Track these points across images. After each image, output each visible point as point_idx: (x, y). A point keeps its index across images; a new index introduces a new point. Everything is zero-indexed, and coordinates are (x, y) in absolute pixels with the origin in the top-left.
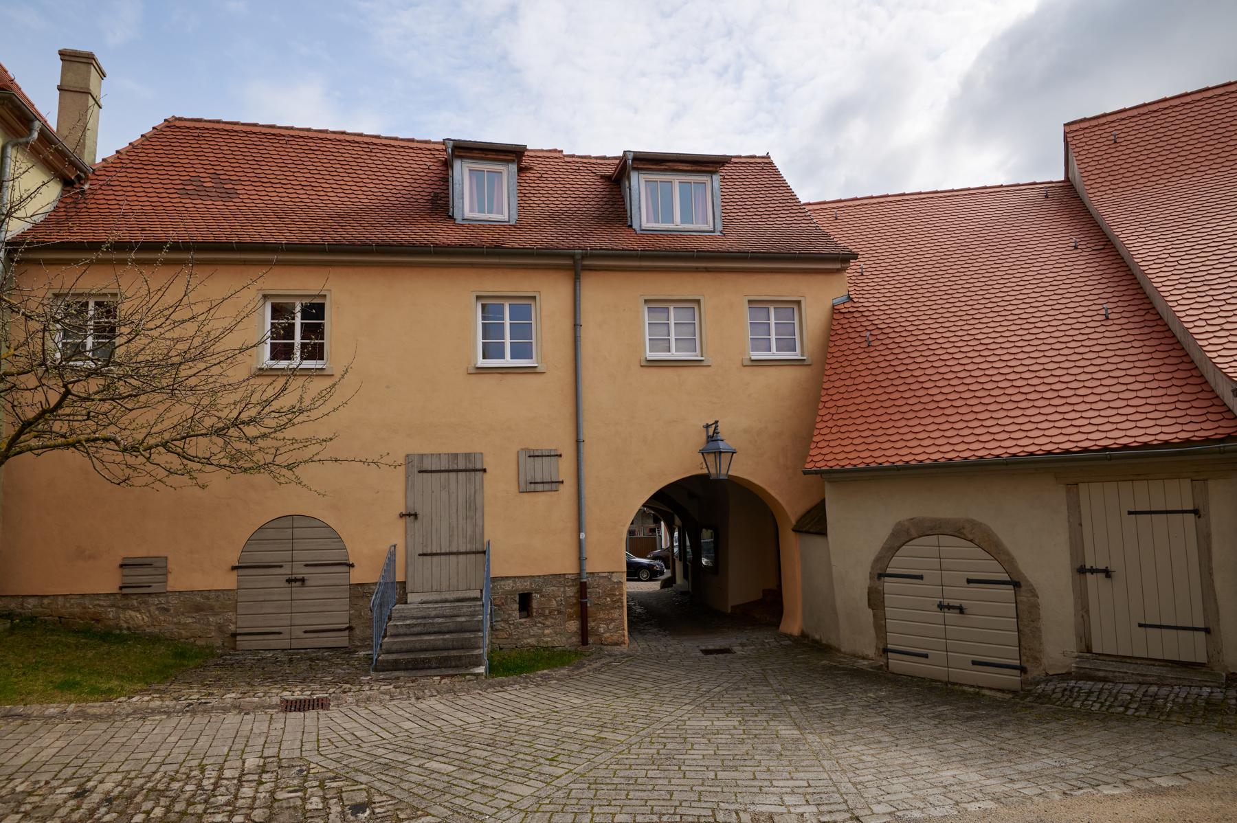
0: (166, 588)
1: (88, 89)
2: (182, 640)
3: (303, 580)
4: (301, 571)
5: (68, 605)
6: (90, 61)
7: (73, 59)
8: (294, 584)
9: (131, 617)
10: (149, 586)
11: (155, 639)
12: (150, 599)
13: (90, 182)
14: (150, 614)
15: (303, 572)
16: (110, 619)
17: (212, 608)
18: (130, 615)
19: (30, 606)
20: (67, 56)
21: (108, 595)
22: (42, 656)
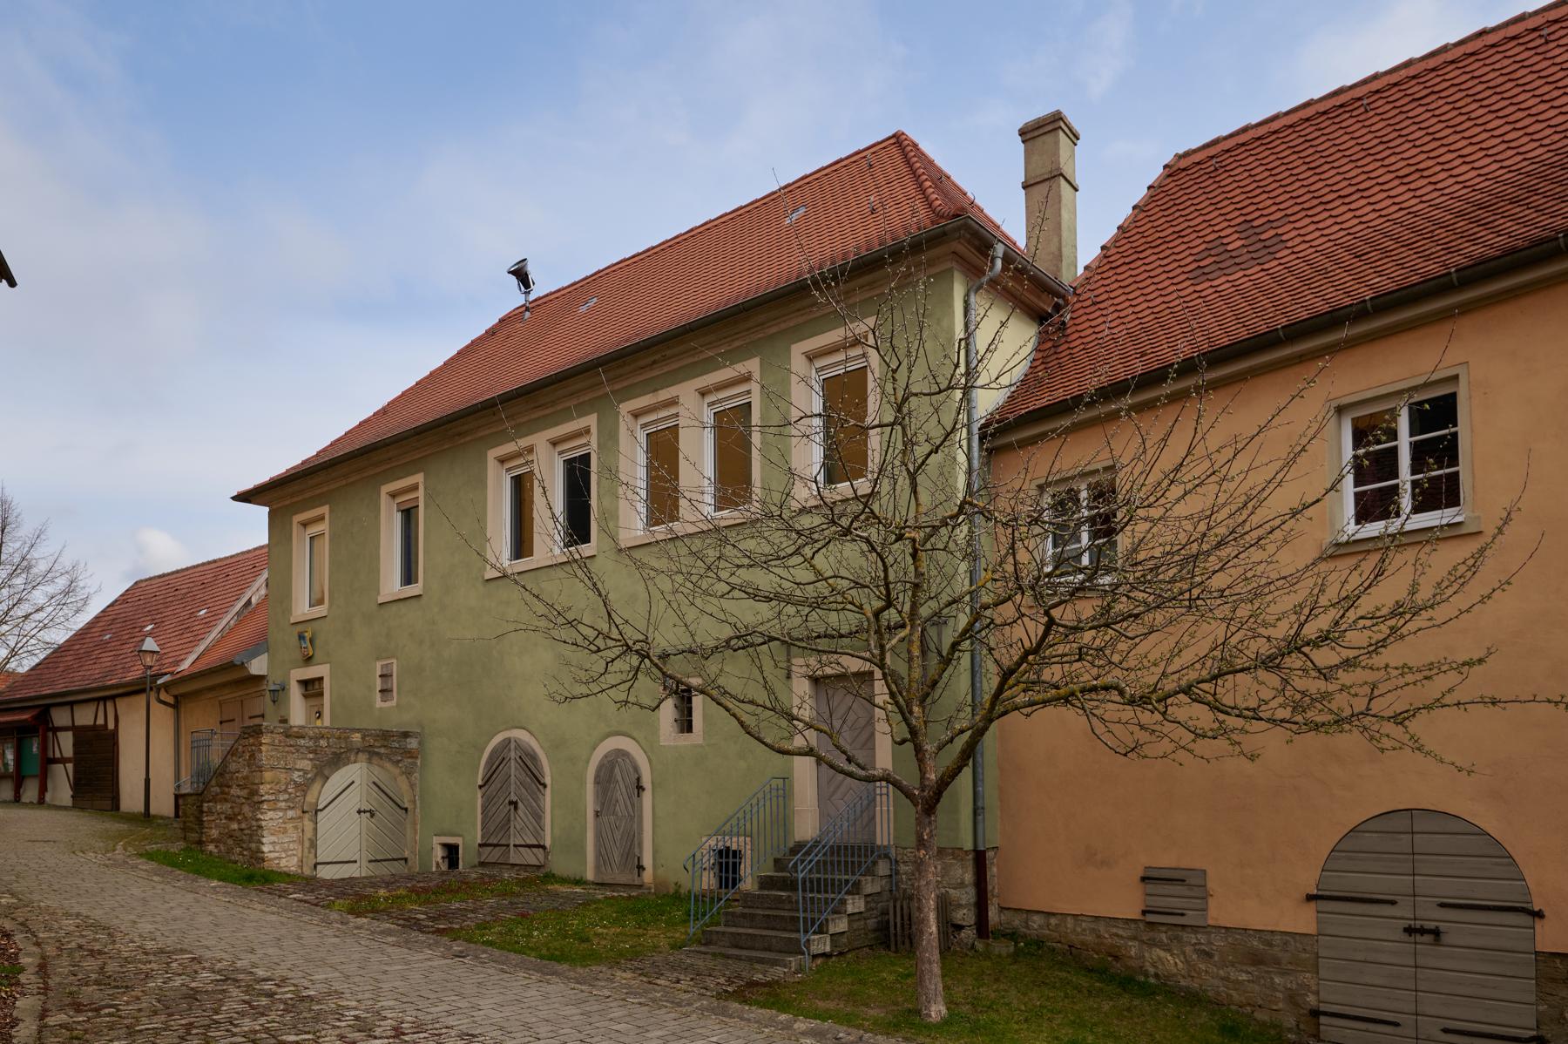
0: (1206, 919)
1: (1059, 168)
3: (1436, 933)
4: (1431, 916)
5: (1079, 930)
7: (1036, 133)
8: (1419, 938)
9: (1160, 959)
10: (1182, 915)
11: (1193, 999)
12: (1185, 935)
14: (1185, 957)
16: (1131, 957)
17: (1277, 962)
19: (1035, 926)
21: (1127, 921)
22: (1048, 999)
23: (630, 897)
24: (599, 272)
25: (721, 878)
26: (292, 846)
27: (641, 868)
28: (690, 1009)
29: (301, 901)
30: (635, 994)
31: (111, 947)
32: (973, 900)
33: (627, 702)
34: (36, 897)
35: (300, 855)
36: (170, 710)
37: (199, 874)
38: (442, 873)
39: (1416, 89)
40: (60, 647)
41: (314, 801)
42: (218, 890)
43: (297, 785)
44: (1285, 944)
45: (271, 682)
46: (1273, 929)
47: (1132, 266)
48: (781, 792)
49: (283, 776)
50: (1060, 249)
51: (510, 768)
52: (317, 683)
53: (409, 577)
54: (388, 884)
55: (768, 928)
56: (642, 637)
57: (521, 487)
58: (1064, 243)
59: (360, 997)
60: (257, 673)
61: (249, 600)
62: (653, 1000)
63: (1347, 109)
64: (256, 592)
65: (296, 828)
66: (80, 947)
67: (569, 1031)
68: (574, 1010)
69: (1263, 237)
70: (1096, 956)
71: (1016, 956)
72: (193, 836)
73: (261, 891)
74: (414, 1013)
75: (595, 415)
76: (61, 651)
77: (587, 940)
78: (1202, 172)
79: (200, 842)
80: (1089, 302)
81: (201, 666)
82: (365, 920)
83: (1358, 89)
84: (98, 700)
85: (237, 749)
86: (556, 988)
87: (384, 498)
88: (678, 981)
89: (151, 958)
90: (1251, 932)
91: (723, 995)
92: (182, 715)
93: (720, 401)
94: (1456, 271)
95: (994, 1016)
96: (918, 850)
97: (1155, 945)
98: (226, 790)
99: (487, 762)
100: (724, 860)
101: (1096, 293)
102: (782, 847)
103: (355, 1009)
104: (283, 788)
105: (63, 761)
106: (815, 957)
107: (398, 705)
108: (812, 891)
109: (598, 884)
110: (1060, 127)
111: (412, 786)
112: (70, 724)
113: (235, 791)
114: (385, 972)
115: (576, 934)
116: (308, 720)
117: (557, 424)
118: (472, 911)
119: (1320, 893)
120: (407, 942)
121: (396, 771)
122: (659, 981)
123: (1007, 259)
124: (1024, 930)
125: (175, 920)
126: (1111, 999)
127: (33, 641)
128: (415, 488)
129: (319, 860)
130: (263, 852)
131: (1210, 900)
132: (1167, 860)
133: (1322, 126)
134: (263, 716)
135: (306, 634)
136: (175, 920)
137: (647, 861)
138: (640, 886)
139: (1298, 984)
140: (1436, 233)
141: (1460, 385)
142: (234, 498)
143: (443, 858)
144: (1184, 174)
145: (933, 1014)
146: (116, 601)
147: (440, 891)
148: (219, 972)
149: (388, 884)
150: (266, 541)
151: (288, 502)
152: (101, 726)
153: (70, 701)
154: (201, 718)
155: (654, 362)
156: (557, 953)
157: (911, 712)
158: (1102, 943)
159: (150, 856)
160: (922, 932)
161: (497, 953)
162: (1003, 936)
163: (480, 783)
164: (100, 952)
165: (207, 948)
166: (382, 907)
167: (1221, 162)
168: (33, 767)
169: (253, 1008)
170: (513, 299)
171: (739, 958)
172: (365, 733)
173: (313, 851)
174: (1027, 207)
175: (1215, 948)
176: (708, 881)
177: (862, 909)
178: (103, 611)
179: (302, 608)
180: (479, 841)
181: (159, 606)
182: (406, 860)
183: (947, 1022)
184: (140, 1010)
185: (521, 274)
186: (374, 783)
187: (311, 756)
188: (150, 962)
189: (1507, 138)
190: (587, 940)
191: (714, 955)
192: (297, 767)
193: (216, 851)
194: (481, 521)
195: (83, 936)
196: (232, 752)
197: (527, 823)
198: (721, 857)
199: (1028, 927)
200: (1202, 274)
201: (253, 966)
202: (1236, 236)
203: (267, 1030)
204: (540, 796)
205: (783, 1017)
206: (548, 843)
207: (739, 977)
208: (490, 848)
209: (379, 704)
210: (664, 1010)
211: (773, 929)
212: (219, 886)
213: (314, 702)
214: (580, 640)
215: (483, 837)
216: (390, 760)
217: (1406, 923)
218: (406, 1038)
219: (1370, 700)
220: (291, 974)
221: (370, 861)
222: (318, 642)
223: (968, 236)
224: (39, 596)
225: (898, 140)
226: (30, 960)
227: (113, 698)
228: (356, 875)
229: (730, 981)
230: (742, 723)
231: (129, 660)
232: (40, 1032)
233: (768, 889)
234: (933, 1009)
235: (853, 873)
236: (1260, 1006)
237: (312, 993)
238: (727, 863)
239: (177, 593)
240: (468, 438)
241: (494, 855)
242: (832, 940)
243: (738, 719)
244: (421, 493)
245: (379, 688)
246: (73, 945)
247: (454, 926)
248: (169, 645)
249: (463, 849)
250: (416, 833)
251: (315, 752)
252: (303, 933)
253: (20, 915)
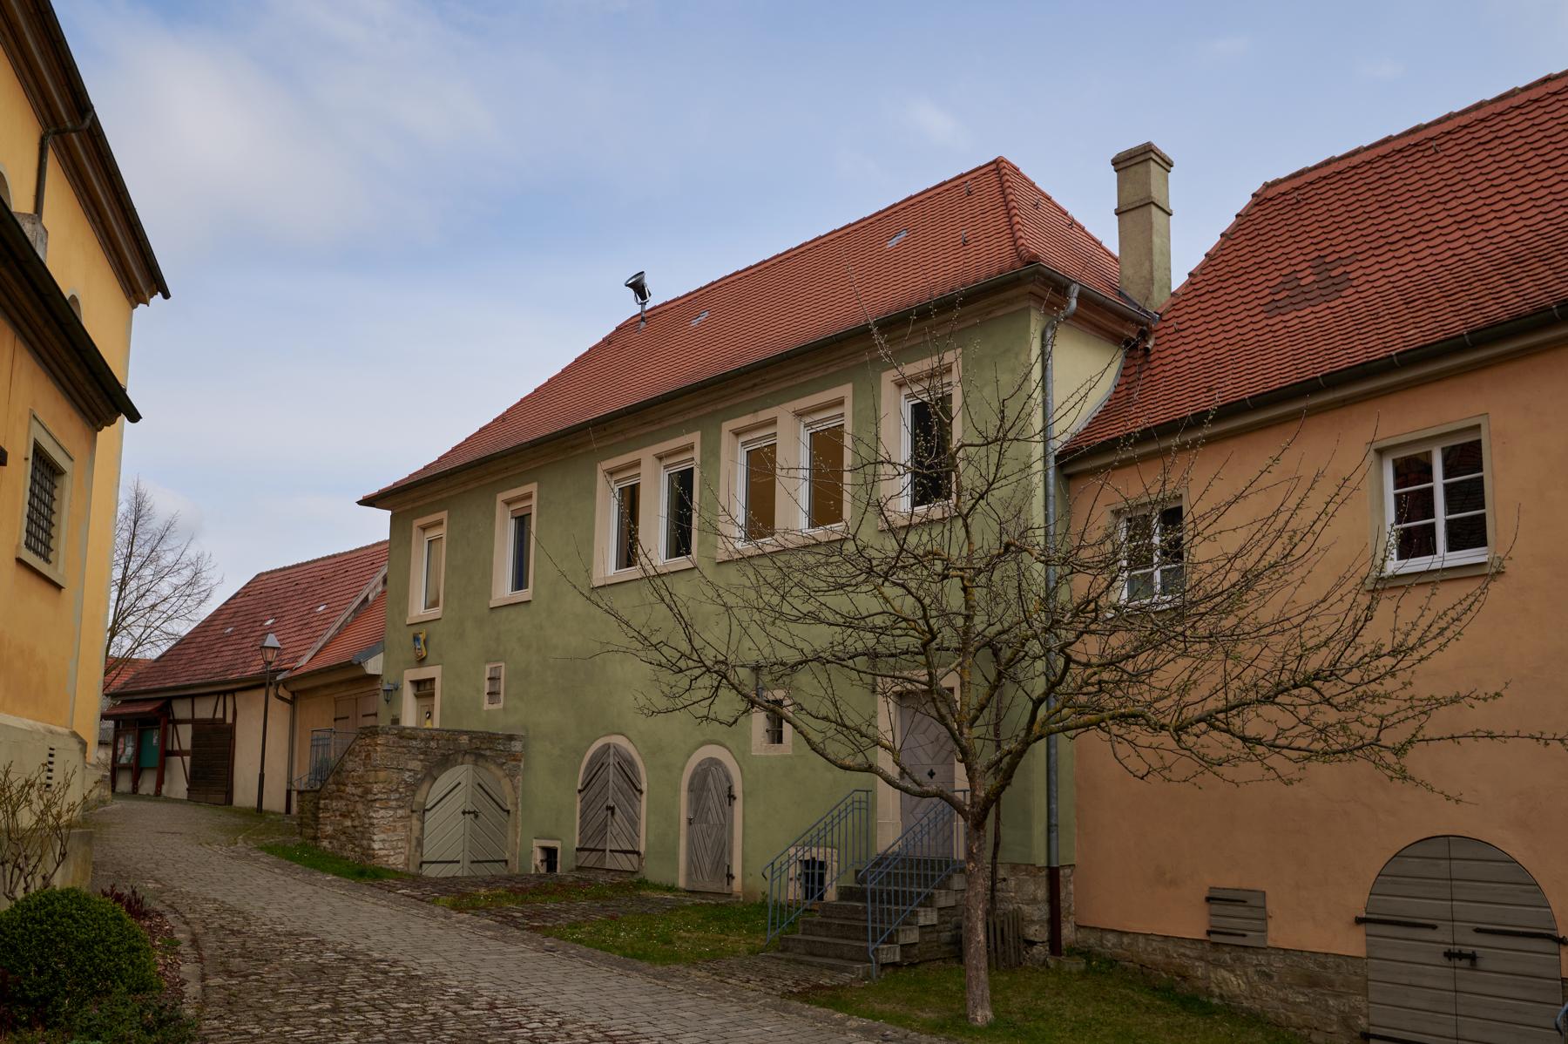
0: (1265, 941)
1: (1150, 197)
2: (1292, 1029)
3: (1473, 958)
4: (1469, 941)
5: (1150, 949)
6: (1147, 156)
7: (1128, 164)
8: (1458, 963)
9: (1224, 979)
10: (1244, 935)
11: (1254, 1019)
12: (1246, 956)
13: (1154, 336)
14: (1247, 978)
15: (1474, 942)
16: (1197, 977)
17: (1331, 984)
18: (1223, 977)
19: (1109, 945)
20: (1123, 163)
21: (1194, 941)
22: (1103, 1012)
23: (717, 905)
24: (713, 283)
25: (807, 889)
26: (400, 844)
27: (730, 877)
28: (753, 1004)
29: (408, 896)
30: (706, 991)
31: (248, 928)
32: (1046, 917)
33: (707, 718)
34: (176, 883)
35: (407, 853)
36: (287, 705)
37: (315, 868)
38: (540, 876)
39: (1483, 133)
40: (182, 640)
41: (422, 801)
42: (333, 883)
43: (408, 785)
44: (1338, 966)
45: (385, 681)
46: (1327, 951)
47: (1215, 295)
48: (864, 805)
49: (395, 776)
50: (1151, 273)
51: (608, 773)
52: (428, 683)
53: (520, 582)
54: (488, 884)
55: (843, 938)
56: (722, 658)
57: (631, 500)
58: (1155, 267)
59: (461, 978)
60: (373, 673)
61: (367, 598)
62: (722, 996)
63: (1420, 148)
64: (373, 588)
65: (404, 826)
66: (222, 927)
67: (639, 1014)
68: (647, 999)
69: (1333, 274)
70: (1164, 976)
71: (1084, 975)
72: (310, 832)
73: (372, 886)
74: (507, 993)
75: (699, 432)
76: (183, 643)
77: (670, 942)
78: (1286, 203)
79: (315, 838)
80: (1172, 330)
81: (319, 664)
82: (466, 916)
83: (1432, 128)
84: (218, 693)
85: (354, 749)
86: (635, 980)
87: (499, 506)
88: (748, 982)
89: (283, 938)
90: (1307, 954)
91: (788, 995)
92: (298, 712)
93: (816, 422)
94: (1468, 333)
95: (1042, 1025)
96: (968, 862)
97: (1220, 966)
98: (342, 788)
99: (587, 768)
100: (810, 871)
101: (1180, 320)
102: (864, 859)
103: (457, 987)
104: (395, 787)
105: (181, 753)
106: (884, 966)
107: (504, 709)
108: (889, 902)
109: (688, 891)
110: (1151, 158)
111: (515, 788)
112: (190, 717)
113: (350, 789)
114: (483, 960)
115: (660, 936)
116: (419, 720)
117: (664, 440)
118: (565, 912)
119: (1369, 916)
120: (504, 936)
121: (500, 773)
122: (730, 981)
123: (1083, 298)
124: (1100, 949)
125: (298, 908)
126: (1168, 1016)
127: (156, 632)
128: (529, 496)
129: (425, 859)
130: (374, 849)
131: (1269, 920)
132: (1230, 881)
133: (1397, 164)
134: (376, 715)
135: (421, 636)
136: (298, 908)
137: (737, 870)
138: (730, 895)
139: (1350, 1006)
140: (1474, 285)
141: (1482, 432)
142: (360, 503)
143: (542, 861)
144: (1270, 203)
145: (979, 1018)
146: (238, 593)
147: (537, 892)
148: (340, 953)
149: (488, 884)
150: (387, 537)
151: (409, 507)
152: (219, 719)
153: (192, 694)
154: (319, 716)
155: (755, 385)
156: (640, 952)
157: (961, 734)
158: (1171, 963)
159: (270, 850)
160: (970, 942)
161: (584, 949)
162: (1078, 954)
163: (579, 787)
164: (239, 932)
165: (329, 932)
166: (483, 904)
167: (1304, 194)
168: (151, 758)
169: (371, 981)
170: (630, 307)
171: (810, 964)
172: (472, 735)
173: (419, 850)
174: (1120, 232)
175: (1274, 969)
176: (794, 892)
177: (935, 921)
178: (225, 604)
179: (418, 609)
180: (577, 845)
181: (280, 601)
182: (506, 862)
183: (991, 1026)
184: (280, 978)
185: (638, 288)
186: (479, 785)
187: (422, 757)
188: (282, 942)
189: (1554, 189)
190: (670, 942)
191: (788, 961)
192: (409, 767)
193: (329, 847)
194: (589, 541)
195: (223, 918)
196: (349, 751)
197: (624, 829)
198: (808, 868)
199: (1102, 946)
200: (1274, 308)
201: (369, 950)
202: (1309, 271)
203: (384, 999)
204: (637, 803)
205: (838, 1015)
206: (642, 849)
207: (807, 980)
208: (587, 853)
209: (486, 706)
210: (729, 1004)
211: (847, 938)
212: (335, 880)
213: (425, 702)
214: (664, 661)
215: (580, 842)
216: (495, 762)
217: (1445, 948)
218: (499, 1011)
219: (1380, 731)
220: (401, 958)
221: (473, 862)
222: (430, 644)
223: (1042, 279)
224: (165, 588)
225: (998, 168)
226: (183, 936)
227: (233, 692)
228: (459, 874)
229: (797, 984)
230: (808, 741)
231: (249, 654)
232: (203, 990)
233: (848, 900)
234: (979, 1013)
235: (927, 886)
236: (1316, 1028)
237: (420, 973)
238: (813, 873)
239: (297, 587)
240: (580, 451)
241: (590, 860)
242: (902, 951)
243: (805, 736)
244: (534, 502)
245: (487, 691)
246: (216, 925)
247: (548, 924)
248: (288, 640)
249: (562, 853)
250: (517, 835)
251: (425, 753)
252: (410, 924)
253: (168, 900)
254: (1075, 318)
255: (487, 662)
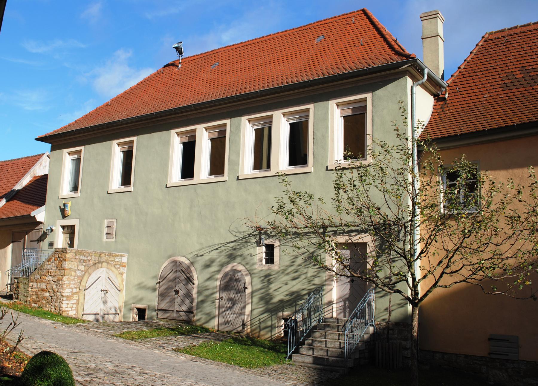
119: (491, 352)
129: (85, 313)
142: (36, 139)
209: (104, 237)
254: (423, 86)
255: (107, 219)
